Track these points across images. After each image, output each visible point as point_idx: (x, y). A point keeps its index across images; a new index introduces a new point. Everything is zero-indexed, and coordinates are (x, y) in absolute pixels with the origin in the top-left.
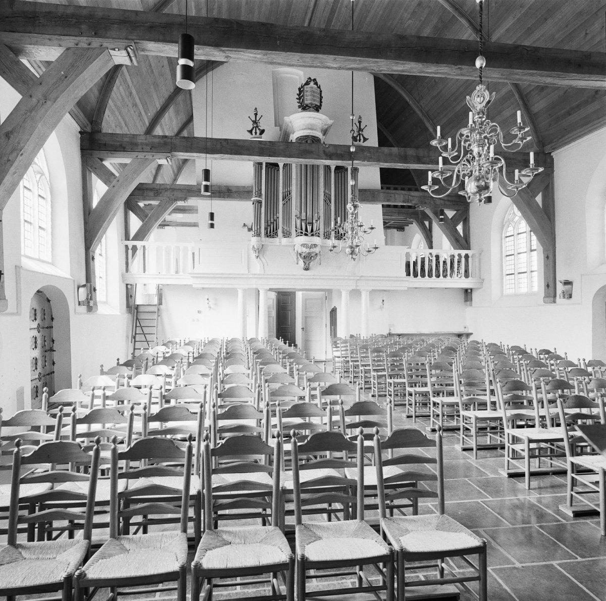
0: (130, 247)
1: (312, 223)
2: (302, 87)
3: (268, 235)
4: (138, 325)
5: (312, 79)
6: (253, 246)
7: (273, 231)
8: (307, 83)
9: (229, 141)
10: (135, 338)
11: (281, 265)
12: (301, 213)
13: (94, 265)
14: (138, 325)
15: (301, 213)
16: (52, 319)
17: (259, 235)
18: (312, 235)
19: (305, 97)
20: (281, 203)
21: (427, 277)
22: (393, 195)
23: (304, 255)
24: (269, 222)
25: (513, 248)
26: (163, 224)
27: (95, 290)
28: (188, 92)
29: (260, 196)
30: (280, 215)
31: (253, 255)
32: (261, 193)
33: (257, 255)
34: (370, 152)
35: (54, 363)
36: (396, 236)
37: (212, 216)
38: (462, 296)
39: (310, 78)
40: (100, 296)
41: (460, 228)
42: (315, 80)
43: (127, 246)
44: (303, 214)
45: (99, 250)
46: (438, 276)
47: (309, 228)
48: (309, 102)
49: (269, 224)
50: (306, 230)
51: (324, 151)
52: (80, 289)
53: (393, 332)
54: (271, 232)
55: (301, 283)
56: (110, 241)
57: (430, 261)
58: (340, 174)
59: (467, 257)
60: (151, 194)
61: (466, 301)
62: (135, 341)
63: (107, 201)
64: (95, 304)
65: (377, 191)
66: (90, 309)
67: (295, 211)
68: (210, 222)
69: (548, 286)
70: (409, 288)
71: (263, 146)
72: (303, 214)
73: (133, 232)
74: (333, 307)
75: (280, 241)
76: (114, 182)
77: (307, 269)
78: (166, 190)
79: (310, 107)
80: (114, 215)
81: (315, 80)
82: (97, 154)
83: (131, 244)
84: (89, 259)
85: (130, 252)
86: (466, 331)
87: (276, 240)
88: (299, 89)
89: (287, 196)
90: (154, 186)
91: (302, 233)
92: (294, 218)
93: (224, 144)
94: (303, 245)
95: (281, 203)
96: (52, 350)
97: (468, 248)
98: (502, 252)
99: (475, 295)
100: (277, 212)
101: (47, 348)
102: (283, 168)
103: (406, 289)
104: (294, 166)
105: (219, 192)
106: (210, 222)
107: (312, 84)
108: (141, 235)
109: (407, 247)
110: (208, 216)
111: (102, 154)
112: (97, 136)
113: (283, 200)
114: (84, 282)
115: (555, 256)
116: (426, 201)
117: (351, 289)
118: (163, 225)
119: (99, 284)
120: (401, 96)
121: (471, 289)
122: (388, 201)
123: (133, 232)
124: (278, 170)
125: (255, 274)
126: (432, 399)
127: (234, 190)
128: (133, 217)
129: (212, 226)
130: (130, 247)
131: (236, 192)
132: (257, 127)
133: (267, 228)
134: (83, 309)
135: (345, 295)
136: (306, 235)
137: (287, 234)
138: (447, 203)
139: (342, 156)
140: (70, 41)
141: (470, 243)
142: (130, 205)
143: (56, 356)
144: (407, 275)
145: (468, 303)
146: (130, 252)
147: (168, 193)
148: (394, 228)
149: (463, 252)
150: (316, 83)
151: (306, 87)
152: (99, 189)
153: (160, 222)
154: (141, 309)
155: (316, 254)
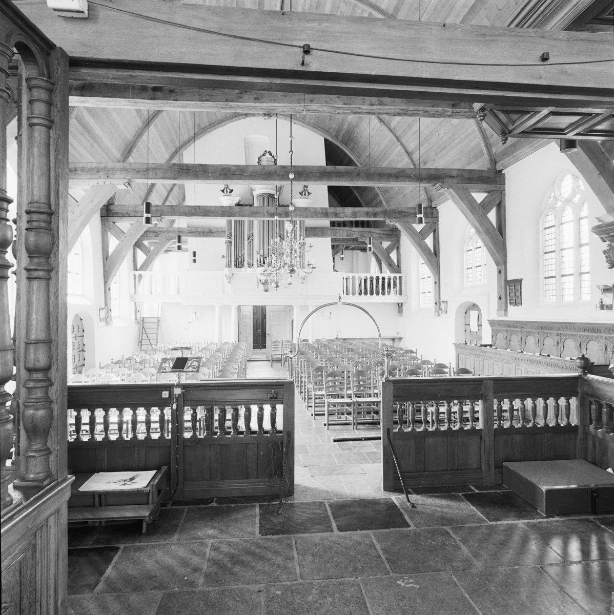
0: (137, 275)
3: (237, 266)
4: (144, 332)
8: (264, 155)
10: (141, 342)
11: (248, 289)
12: (260, 250)
13: (110, 294)
14: (144, 332)
15: (260, 250)
16: (83, 331)
17: (229, 266)
20: (246, 242)
22: (338, 231)
25: (554, 243)
26: (168, 249)
27: (110, 310)
28: (70, 391)
29: (230, 237)
30: (246, 251)
31: (226, 281)
32: (231, 236)
34: (301, 211)
35: (84, 359)
36: (359, 255)
37: (194, 253)
40: (114, 313)
41: (393, 255)
43: (135, 275)
45: (113, 285)
46: (372, 294)
52: (101, 311)
53: (339, 337)
54: (239, 264)
55: (271, 300)
56: (124, 271)
57: (372, 281)
59: (400, 278)
60: (153, 235)
61: (399, 312)
62: (141, 345)
63: (118, 251)
64: (111, 320)
65: (327, 228)
66: (107, 323)
67: (256, 248)
68: (194, 258)
69: (500, 298)
72: (262, 251)
73: (140, 263)
75: (245, 271)
76: (123, 238)
78: (164, 232)
80: (123, 260)
81: (269, 152)
82: (111, 219)
83: (137, 273)
84: (107, 290)
85: (137, 279)
86: (398, 336)
87: (243, 269)
88: (259, 159)
89: (251, 237)
90: (155, 229)
92: (255, 254)
93: (197, 209)
95: (246, 242)
96: (83, 351)
98: (419, 275)
99: (404, 307)
101: (81, 349)
104: (246, 221)
105: (203, 232)
106: (194, 258)
107: (268, 154)
108: (145, 266)
110: (192, 254)
111: (115, 219)
112: (112, 207)
114: (103, 306)
115: (439, 281)
116: (365, 235)
118: (167, 251)
119: (114, 304)
120: (346, 154)
121: (402, 304)
122: (335, 235)
123: (140, 263)
127: (214, 230)
128: (139, 252)
129: (195, 261)
130: (137, 275)
131: (216, 232)
132: (228, 187)
134: (103, 323)
137: (251, 265)
138: (382, 236)
140: (94, 182)
142: (138, 245)
143: (86, 354)
146: (137, 279)
147: (165, 234)
148: (358, 249)
149: (398, 275)
150: (271, 154)
152: (113, 243)
153: (165, 248)
154: (146, 320)
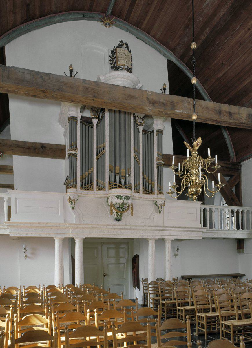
1: (125, 177)
2: (115, 49)
5: (124, 42)
6: (70, 197)
7: (88, 184)
8: (120, 46)
9: (51, 76)
18: (126, 188)
19: (118, 59)
21: (241, 229)
23: (117, 206)
24: (84, 175)
33: (73, 206)
38: (235, 246)
39: (122, 42)
42: (126, 44)
44: (117, 168)
47: (123, 181)
48: (122, 63)
49: (84, 177)
50: (120, 183)
51: (148, 98)
58: (146, 135)
70: (203, 238)
71: (87, 85)
74: (135, 255)
77: (118, 220)
79: (122, 69)
88: (112, 51)
91: (116, 185)
94: (118, 197)
97: (240, 205)
100: (92, 166)
102: (97, 125)
103: (201, 238)
109: (202, 202)
113: (97, 155)
117: (157, 238)
124: (92, 127)
125: (71, 224)
126: (161, 302)
133: (82, 181)
135: (151, 246)
136: (120, 187)
137: (101, 187)
139: (165, 105)
141: (242, 202)
144: (8, 221)
145: (241, 250)
150: (127, 48)
151: (118, 49)
155: (128, 207)
